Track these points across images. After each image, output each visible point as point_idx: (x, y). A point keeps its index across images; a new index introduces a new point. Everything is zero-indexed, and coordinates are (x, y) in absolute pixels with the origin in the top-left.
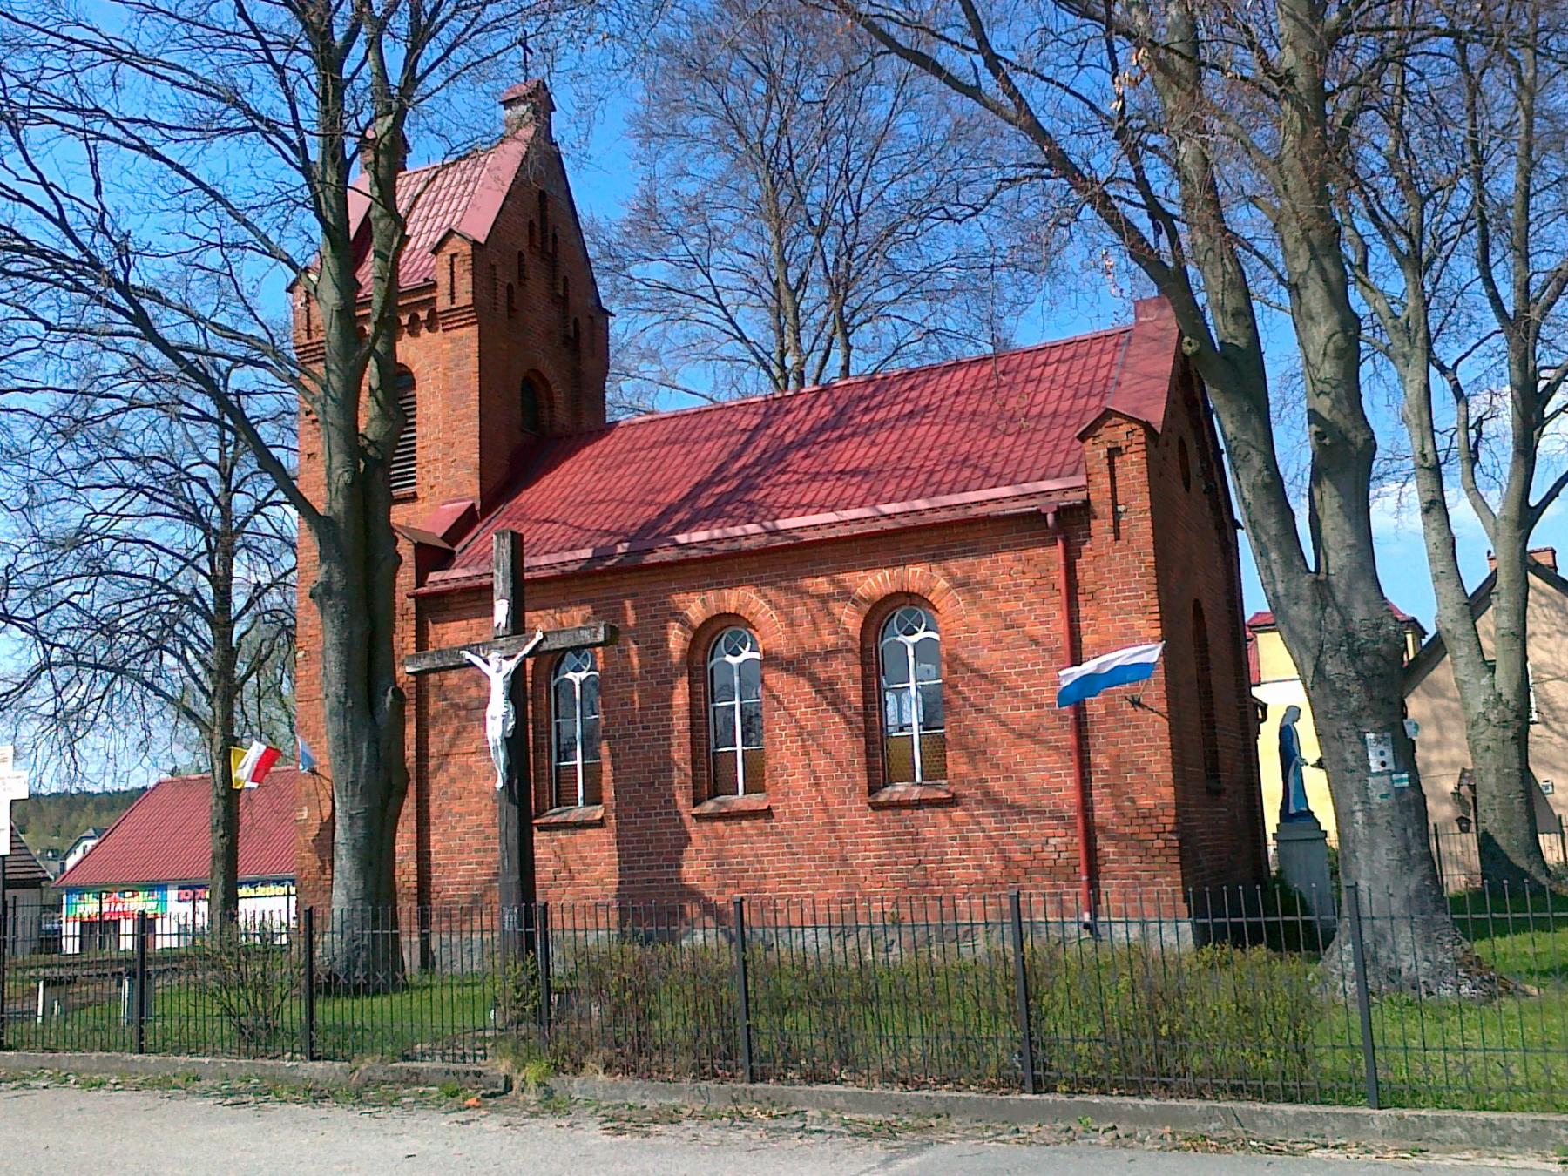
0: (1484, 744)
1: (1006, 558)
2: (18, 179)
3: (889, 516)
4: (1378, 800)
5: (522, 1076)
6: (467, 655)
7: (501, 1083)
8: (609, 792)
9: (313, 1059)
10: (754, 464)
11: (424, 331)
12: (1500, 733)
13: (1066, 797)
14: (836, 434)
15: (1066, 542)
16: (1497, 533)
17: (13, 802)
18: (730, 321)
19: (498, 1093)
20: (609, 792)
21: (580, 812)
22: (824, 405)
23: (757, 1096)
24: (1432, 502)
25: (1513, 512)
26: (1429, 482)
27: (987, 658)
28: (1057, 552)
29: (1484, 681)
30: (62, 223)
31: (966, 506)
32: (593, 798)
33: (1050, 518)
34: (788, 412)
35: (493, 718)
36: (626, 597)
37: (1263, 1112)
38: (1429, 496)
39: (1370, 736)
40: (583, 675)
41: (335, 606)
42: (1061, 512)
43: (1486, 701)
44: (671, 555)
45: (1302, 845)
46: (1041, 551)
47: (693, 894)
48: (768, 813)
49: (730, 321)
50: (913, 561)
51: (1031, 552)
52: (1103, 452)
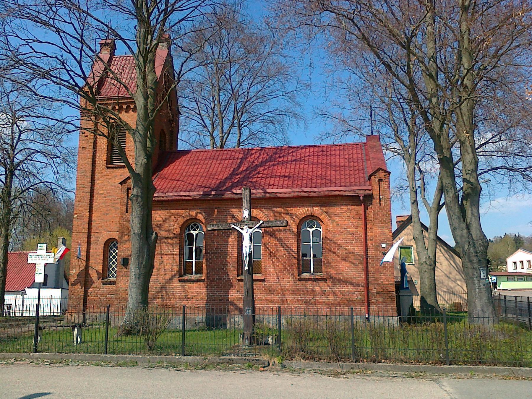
0: (425, 270)
1: (344, 208)
2: (71, 46)
3: (305, 192)
4: (483, 286)
5: (272, 361)
6: (233, 226)
7: (267, 363)
8: (205, 271)
9: (185, 355)
10: (246, 170)
11: (131, 112)
12: (429, 267)
13: (361, 280)
14: (271, 163)
15: (364, 205)
16: (431, 211)
17: (46, 264)
18: (203, 120)
19: (266, 366)
20: (205, 271)
21: (194, 277)
22: (264, 154)
23: (360, 367)
24: (415, 201)
25: (435, 206)
26: (414, 195)
27: (338, 237)
28: (361, 208)
29: (426, 252)
30: (80, 63)
31: (330, 191)
32: (199, 271)
33: (361, 198)
34: (252, 155)
35: (246, 247)
36: (216, 208)
37: (520, 369)
38: (414, 199)
39: (481, 268)
40: (197, 232)
41: (139, 203)
42: (365, 196)
43: (426, 258)
44: (230, 197)
45: (407, 297)
46: (356, 207)
47: (233, 304)
48: (263, 280)
49: (203, 120)
50: (315, 206)
51: (353, 207)
52: (377, 180)
